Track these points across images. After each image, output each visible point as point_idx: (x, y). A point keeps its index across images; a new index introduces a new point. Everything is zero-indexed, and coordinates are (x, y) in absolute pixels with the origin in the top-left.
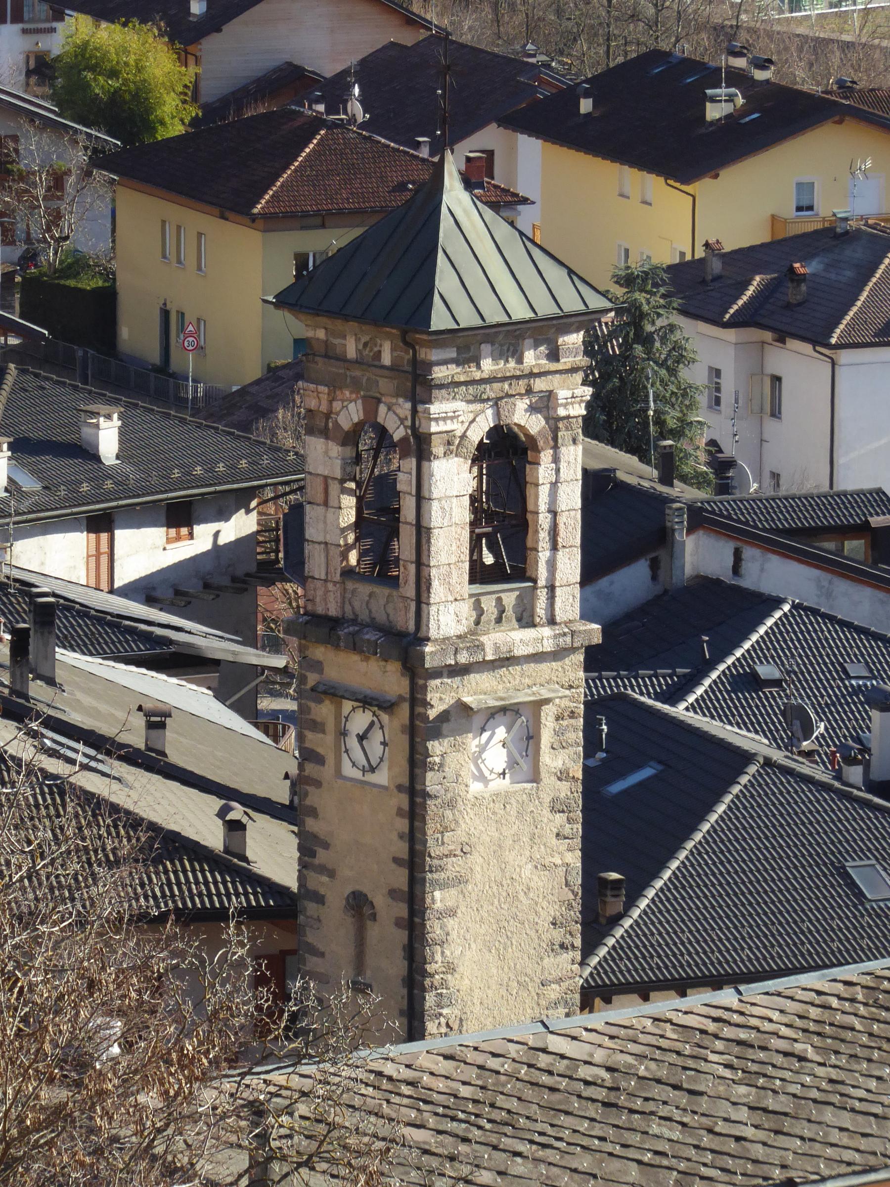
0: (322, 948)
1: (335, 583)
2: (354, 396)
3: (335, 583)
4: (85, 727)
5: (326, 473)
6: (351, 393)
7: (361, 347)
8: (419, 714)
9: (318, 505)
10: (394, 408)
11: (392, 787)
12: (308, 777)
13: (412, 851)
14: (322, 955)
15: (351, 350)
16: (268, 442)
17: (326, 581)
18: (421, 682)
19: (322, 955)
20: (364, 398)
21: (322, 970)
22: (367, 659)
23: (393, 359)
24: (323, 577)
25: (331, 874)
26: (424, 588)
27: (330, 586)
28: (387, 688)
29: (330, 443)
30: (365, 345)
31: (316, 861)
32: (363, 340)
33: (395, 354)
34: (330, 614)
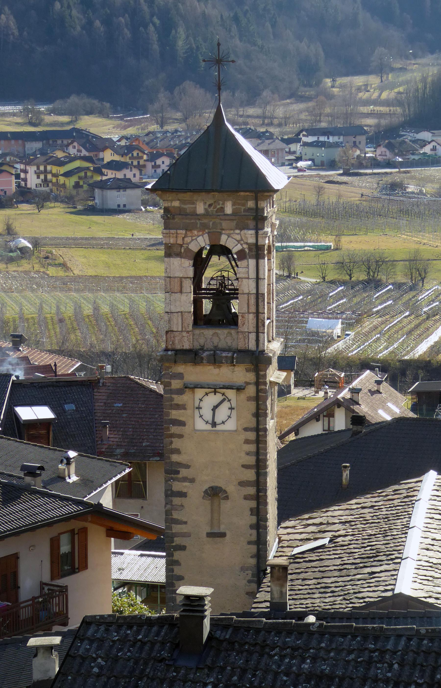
0: (185, 520)
1: (188, 332)
2: (201, 233)
3: (188, 332)
4: (276, 504)
5: (181, 276)
6: (198, 232)
7: (207, 207)
8: (262, 389)
9: (177, 293)
10: (232, 235)
11: (240, 429)
12: (173, 434)
13: (258, 461)
14: (186, 523)
15: (200, 209)
16: (175, 235)
17: (182, 331)
18: (262, 373)
19: (186, 523)
20: (208, 233)
21: (185, 531)
22: (219, 367)
23: (233, 210)
24: (180, 329)
25: (192, 481)
26: (260, 324)
27: (184, 334)
28: (235, 380)
29: (183, 260)
30: (210, 205)
31: (180, 476)
32: (208, 203)
33: (234, 207)
34: (185, 348)
